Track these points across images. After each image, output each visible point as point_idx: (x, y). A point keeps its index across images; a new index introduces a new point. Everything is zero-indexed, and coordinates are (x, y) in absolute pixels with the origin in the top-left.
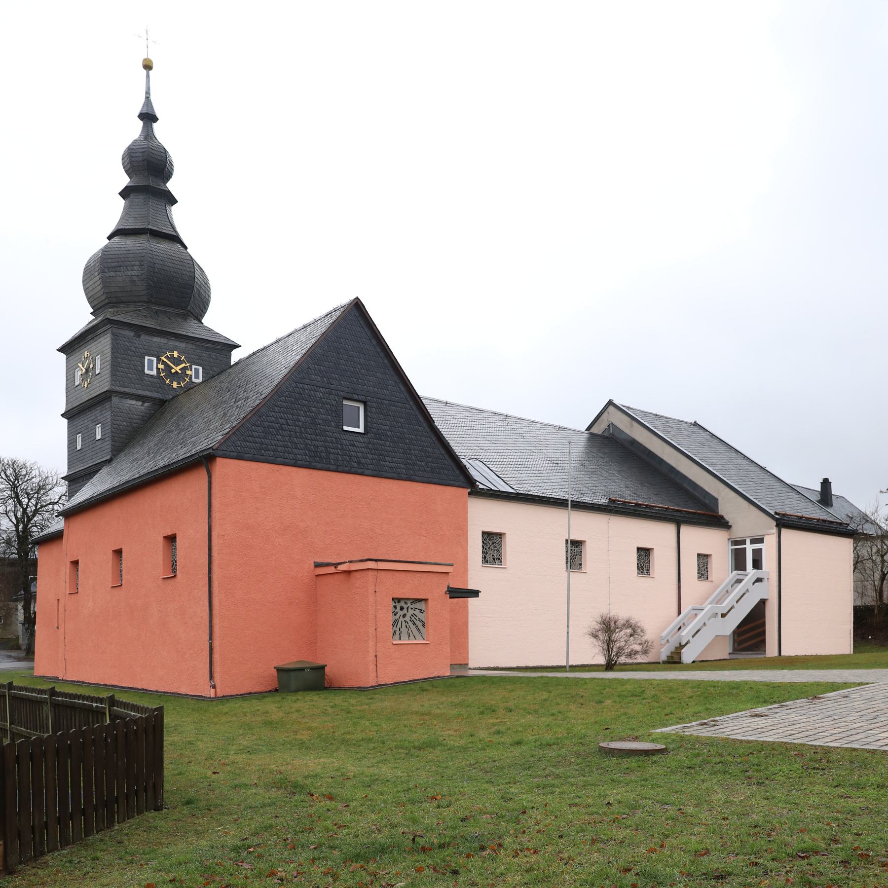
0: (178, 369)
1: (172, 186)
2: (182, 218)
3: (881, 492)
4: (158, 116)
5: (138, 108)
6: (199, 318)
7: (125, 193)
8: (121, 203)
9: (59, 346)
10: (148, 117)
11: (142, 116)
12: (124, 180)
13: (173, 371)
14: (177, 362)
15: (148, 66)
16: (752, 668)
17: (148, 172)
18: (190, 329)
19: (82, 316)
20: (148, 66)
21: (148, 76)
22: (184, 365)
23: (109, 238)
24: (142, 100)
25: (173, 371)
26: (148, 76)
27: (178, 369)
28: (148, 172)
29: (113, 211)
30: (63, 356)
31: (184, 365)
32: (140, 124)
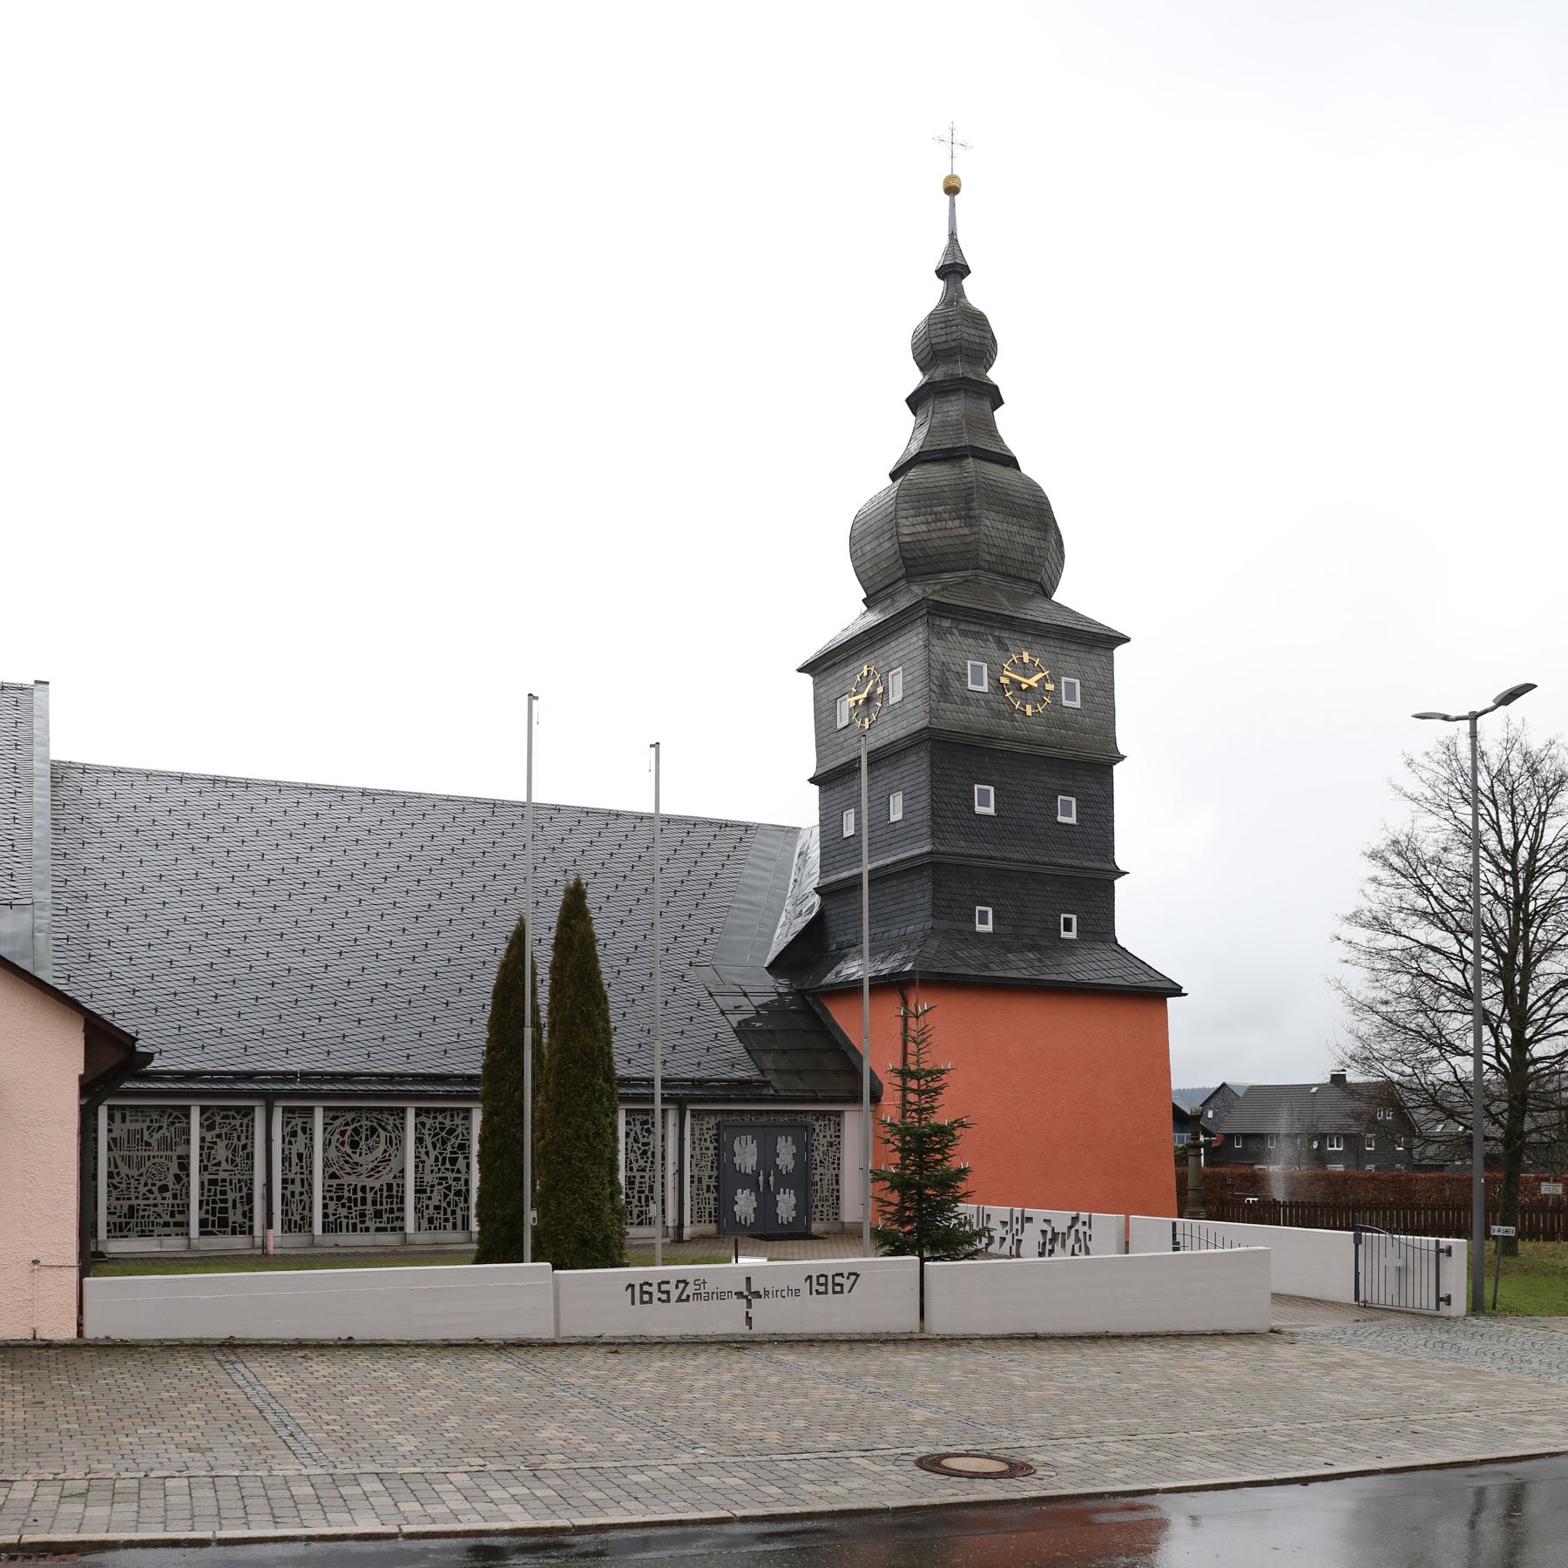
0: (1032, 681)
1: (996, 374)
2: (1010, 425)
3: (748, 1279)
4: (1166, 964)
5: (936, 258)
6: (1045, 590)
7: (915, 402)
8: (908, 419)
9: (799, 665)
10: (953, 270)
11: (942, 273)
12: (914, 378)
13: (1024, 686)
14: (1027, 670)
15: (952, 190)
16: (91, 1542)
17: (955, 359)
18: (1035, 612)
19: (842, 608)
20: (952, 190)
21: (953, 205)
22: (1040, 675)
23: (894, 476)
24: (945, 241)
25: (1024, 686)
26: (953, 205)
27: (1032, 681)
28: (955, 359)
29: (899, 433)
30: (807, 679)
31: (1040, 675)
32: (940, 285)
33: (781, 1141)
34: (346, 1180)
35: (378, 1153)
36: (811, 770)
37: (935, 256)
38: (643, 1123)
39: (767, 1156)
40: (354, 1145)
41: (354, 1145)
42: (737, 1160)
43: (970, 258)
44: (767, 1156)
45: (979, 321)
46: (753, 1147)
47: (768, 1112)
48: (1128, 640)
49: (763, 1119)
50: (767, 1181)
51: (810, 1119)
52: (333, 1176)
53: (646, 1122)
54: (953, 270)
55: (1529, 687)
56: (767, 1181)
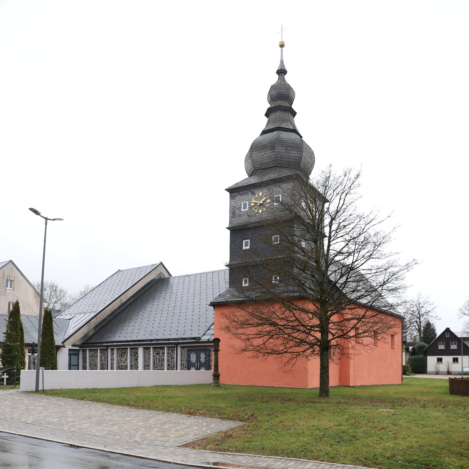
1: (294, 107)
8: (266, 119)
10: (282, 72)
15: (282, 46)
17: (281, 101)
20: (282, 46)
23: (267, 115)
28: (281, 101)
33: (202, 354)
34: (120, 364)
35: (125, 358)
36: (227, 225)
37: (277, 67)
38: (172, 350)
39: (198, 358)
40: (122, 356)
41: (122, 356)
42: (191, 359)
43: (287, 68)
44: (198, 358)
45: (289, 88)
46: (195, 356)
47: (199, 346)
48: (225, 190)
49: (198, 348)
50: (197, 365)
51: (210, 348)
52: (118, 363)
53: (172, 350)
54: (282, 72)
55: (62, 220)
56: (197, 365)
